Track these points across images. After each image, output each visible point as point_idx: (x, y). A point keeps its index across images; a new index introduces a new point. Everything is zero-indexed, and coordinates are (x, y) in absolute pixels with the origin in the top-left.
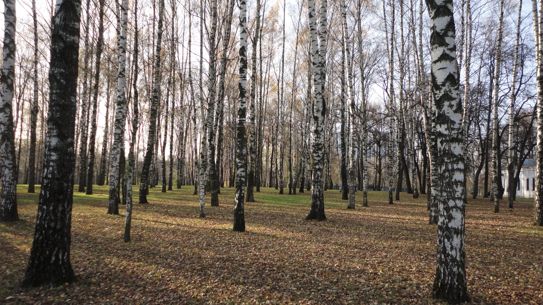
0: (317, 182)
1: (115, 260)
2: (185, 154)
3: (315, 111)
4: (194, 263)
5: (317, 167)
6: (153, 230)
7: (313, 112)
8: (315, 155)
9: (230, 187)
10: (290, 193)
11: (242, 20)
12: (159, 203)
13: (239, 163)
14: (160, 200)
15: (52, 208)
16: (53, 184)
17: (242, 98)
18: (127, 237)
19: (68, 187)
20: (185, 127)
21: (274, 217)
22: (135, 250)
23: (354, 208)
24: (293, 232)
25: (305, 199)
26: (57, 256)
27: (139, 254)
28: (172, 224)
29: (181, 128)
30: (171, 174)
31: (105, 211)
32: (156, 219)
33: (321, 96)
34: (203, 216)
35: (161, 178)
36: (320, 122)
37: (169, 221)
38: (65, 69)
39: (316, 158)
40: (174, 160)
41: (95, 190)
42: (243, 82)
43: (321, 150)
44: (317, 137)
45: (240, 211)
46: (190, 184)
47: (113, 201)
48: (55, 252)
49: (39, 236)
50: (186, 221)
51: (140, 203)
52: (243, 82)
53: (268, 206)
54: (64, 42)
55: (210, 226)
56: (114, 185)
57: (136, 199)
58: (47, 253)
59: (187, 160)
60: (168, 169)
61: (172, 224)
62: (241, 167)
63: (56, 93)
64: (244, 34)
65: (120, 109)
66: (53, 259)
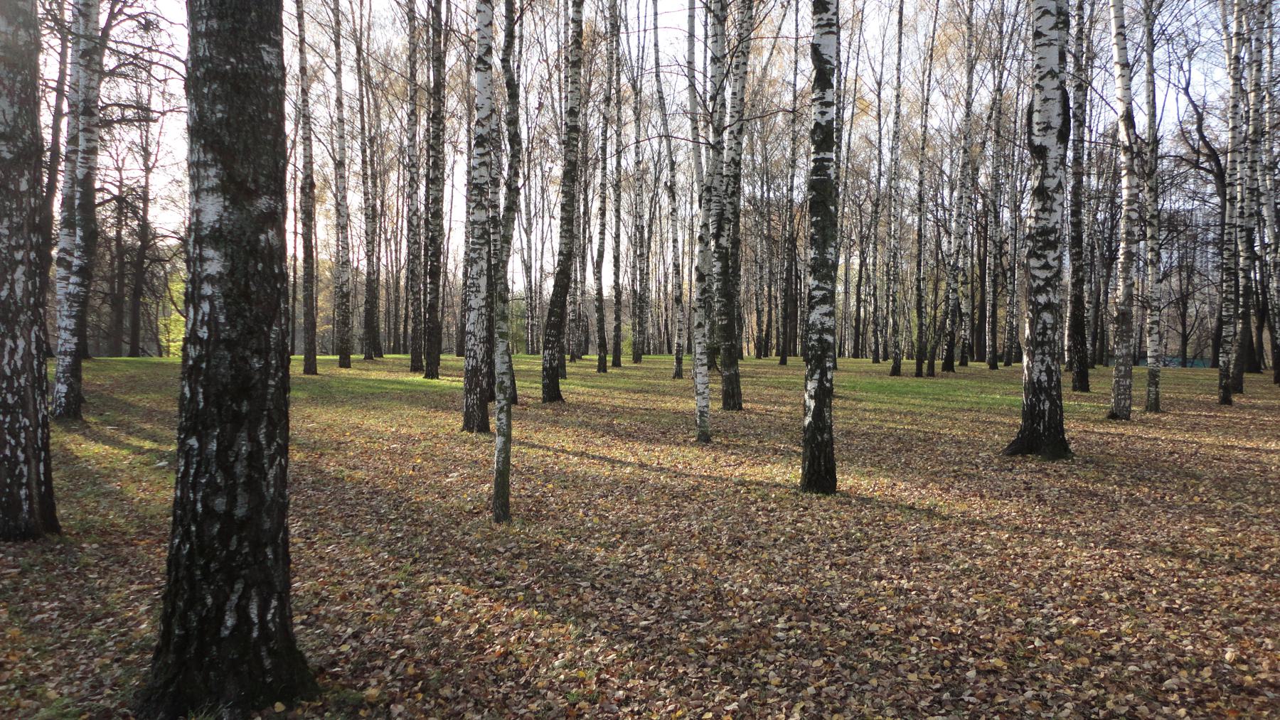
0: (1042, 344)
1: (457, 593)
2: (648, 280)
3: (1036, 128)
4: (701, 619)
5: (1042, 299)
6: (572, 482)
7: (1030, 133)
9: (758, 356)
10: (919, 374)
13: (818, 288)
14: (594, 391)
15: (213, 446)
16: (213, 362)
17: (823, 90)
18: (501, 506)
19: (265, 369)
20: (647, 217)
21: (904, 444)
22: (519, 556)
23: (1128, 418)
24: (982, 497)
25: (966, 388)
26: (242, 612)
27: (529, 571)
28: (625, 464)
30: (618, 329)
31: (455, 421)
32: (581, 448)
33: (1056, 83)
34: (704, 439)
35: (594, 338)
36: (1051, 164)
37: (616, 453)
39: (1037, 273)
40: (624, 297)
41: (446, 368)
43: (1055, 248)
44: (1043, 210)
45: (822, 431)
46: (661, 352)
47: (473, 399)
48: (234, 598)
49: (182, 542)
50: (662, 455)
51: (544, 400)
53: (875, 410)
55: (729, 470)
56: (474, 357)
57: (530, 389)
58: (209, 600)
59: (653, 296)
61: (625, 464)
62: (824, 300)
63: (208, 34)
65: (482, 155)
66: (230, 621)
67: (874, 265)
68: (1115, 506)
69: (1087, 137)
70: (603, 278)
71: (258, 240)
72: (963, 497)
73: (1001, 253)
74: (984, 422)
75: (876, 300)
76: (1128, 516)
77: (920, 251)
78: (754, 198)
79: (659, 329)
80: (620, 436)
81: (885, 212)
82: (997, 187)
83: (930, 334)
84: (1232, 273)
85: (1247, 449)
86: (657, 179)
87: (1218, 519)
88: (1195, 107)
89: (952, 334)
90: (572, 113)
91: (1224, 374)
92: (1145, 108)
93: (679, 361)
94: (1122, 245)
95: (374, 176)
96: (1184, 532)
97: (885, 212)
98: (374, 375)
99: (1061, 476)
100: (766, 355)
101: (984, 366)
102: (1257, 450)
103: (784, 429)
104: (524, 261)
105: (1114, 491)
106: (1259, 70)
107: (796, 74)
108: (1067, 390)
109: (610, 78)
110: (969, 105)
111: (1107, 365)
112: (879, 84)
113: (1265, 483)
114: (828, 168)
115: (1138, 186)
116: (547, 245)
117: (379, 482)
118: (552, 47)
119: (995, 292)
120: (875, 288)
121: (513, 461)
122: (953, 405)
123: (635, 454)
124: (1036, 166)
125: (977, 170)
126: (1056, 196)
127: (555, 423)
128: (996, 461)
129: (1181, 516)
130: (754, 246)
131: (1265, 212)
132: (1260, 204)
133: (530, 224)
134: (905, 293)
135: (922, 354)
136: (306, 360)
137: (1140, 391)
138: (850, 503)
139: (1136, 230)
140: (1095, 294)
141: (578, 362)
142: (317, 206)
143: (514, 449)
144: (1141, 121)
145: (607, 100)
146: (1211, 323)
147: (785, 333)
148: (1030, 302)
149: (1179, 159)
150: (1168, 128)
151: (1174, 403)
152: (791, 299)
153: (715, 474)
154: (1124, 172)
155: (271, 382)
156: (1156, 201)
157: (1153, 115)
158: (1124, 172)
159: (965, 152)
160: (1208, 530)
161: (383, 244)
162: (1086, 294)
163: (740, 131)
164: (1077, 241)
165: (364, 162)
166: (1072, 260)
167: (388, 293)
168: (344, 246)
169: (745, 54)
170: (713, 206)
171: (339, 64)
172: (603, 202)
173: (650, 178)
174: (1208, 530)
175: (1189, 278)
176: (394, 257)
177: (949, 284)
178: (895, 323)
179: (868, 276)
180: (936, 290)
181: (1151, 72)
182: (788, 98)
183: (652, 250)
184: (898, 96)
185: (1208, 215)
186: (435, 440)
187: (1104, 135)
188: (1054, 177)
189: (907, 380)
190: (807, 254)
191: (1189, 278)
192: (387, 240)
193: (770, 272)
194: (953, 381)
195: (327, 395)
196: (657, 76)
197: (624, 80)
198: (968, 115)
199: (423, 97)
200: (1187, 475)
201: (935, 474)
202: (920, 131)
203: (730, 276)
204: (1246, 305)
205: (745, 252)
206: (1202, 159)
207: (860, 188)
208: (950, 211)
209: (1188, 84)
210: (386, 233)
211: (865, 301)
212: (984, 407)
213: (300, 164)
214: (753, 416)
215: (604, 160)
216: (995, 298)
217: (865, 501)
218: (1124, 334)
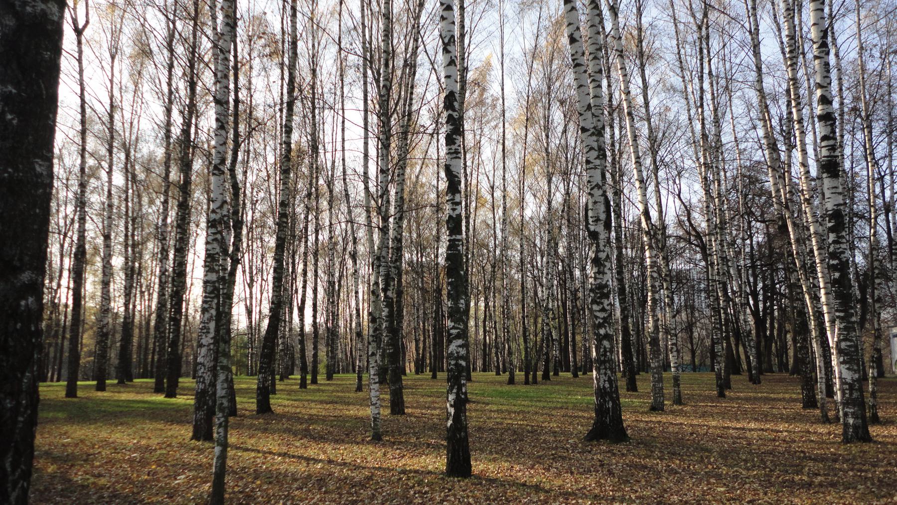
0: (604, 362)
2: (338, 319)
3: (590, 220)
5: (602, 331)
6: (276, 478)
7: (587, 223)
8: (595, 307)
9: (417, 373)
11: (446, 41)
12: (293, 410)
17: (453, 194)
20: (337, 275)
21: (518, 435)
24: (572, 473)
28: (317, 461)
29: (331, 274)
30: (315, 356)
31: (186, 432)
32: (284, 449)
33: (601, 192)
34: (377, 438)
35: (298, 362)
36: (602, 243)
38: (17, 85)
39: (598, 314)
40: (321, 332)
41: (184, 389)
42: (454, 162)
44: (599, 272)
46: (348, 372)
50: (346, 453)
51: (258, 412)
52: (454, 162)
53: (498, 411)
54: (17, 15)
56: (203, 382)
57: (247, 404)
59: (342, 330)
60: (309, 346)
61: (317, 461)
62: (458, 336)
64: (452, 67)
65: (214, 234)
67: (494, 307)
68: (658, 475)
69: (623, 225)
70: (306, 318)
71: (19, 305)
72: (559, 475)
73: (575, 298)
74: (571, 416)
75: (496, 331)
76: (668, 482)
77: (523, 297)
78: (412, 262)
79: (346, 354)
80: (314, 439)
81: (500, 271)
82: (571, 256)
83: (533, 354)
84: (716, 310)
85: (737, 429)
86: (345, 249)
87: (724, 481)
88: (686, 207)
89: (547, 354)
90: (283, 204)
91: (719, 376)
92: (656, 207)
93: (360, 378)
94: (649, 294)
95: (134, 248)
96: (704, 491)
97: (500, 271)
98: (124, 396)
99: (623, 455)
100: (422, 372)
101: (569, 375)
102: (743, 429)
103: (434, 428)
104: (246, 307)
105: (658, 464)
106: (719, 185)
107: (438, 181)
108: (622, 391)
109: (311, 181)
110: (550, 203)
111: (647, 372)
112: (492, 188)
113: (750, 453)
114: (458, 245)
115: (656, 255)
116: (265, 294)
117: (118, 486)
118: (271, 159)
119: (573, 324)
120: (495, 323)
121: (230, 463)
122: (550, 405)
123: (325, 452)
124: (592, 244)
125: (557, 244)
126: (606, 264)
127: (265, 430)
128: (580, 445)
129: (701, 480)
130: (412, 296)
131: (732, 272)
132: (728, 267)
133: (252, 280)
134: (516, 326)
135: (528, 367)
136: (68, 386)
137: (669, 390)
138: (481, 484)
139: (657, 284)
140: (636, 325)
141: (286, 381)
142: (88, 267)
143: (231, 453)
144: (654, 214)
145: (309, 195)
146: (708, 342)
147: (435, 356)
148: (595, 334)
149: (679, 238)
150: (670, 219)
151: (691, 397)
152: (439, 330)
153: (385, 466)
154: (647, 247)
155: (21, 419)
156: (668, 265)
157: (661, 212)
158: (647, 247)
159: (549, 233)
160: (719, 489)
161: (138, 295)
162: (630, 325)
163: (401, 219)
164: (622, 291)
165: (126, 236)
166: (620, 303)
167: (141, 332)
168: (106, 297)
169: (403, 168)
170: (381, 269)
171: (111, 167)
172: (305, 265)
173: (339, 248)
174: (719, 489)
175: (692, 313)
176: (146, 305)
177: (543, 320)
178: (509, 348)
179: (491, 315)
180: (536, 323)
181: (657, 184)
182: (433, 196)
183: (337, 300)
184: (504, 197)
185: (700, 272)
186: (168, 449)
187: (633, 223)
188: (604, 251)
189: (519, 387)
190: (447, 303)
191: (692, 313)
192: (142, 293)
193: (424, 313)
194: (550, 387)
195: (83, 414)
196: (344, 179)
197: (321, 182)
198: (549, 209)
199: (174, 191)
200: (702, 449)
201: (540, 457)
202: (520, 218)
203: (395, 316)
204: (727, 332)
205: (406, 299)
206: (692, 238)
207: (482, 255)
208: (542, 270)
209: (680, 192)
210: (141, 286)
211: (489, 332)
212: (571, 406)
213: (75, 238)
214: (413, 419)
215: (306, 238)
216: (574, 329)
217: (492, 481)
218: (656, 352)
